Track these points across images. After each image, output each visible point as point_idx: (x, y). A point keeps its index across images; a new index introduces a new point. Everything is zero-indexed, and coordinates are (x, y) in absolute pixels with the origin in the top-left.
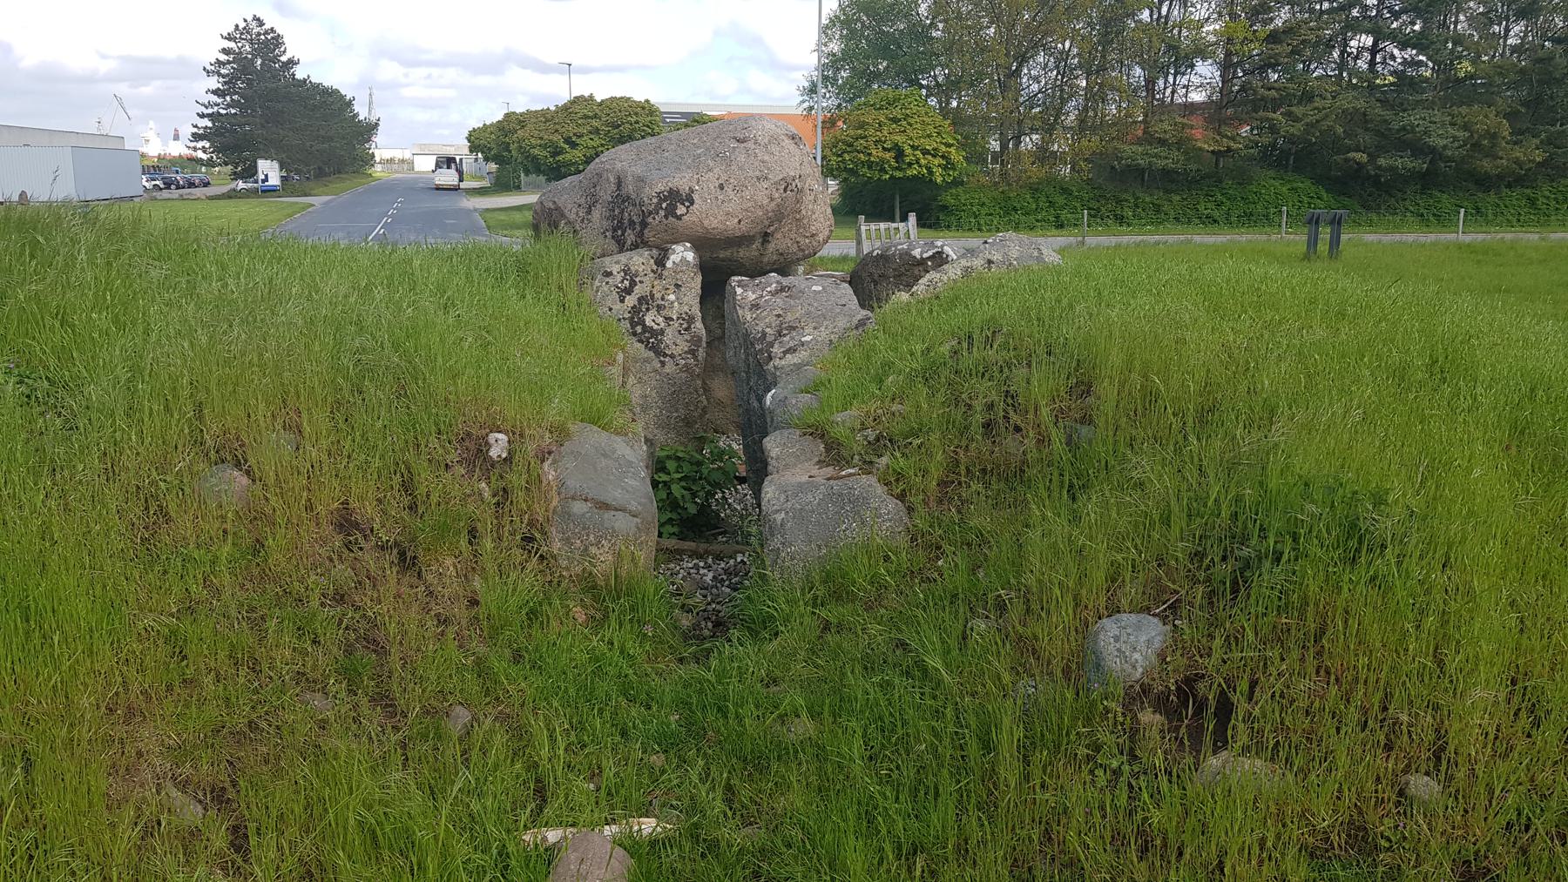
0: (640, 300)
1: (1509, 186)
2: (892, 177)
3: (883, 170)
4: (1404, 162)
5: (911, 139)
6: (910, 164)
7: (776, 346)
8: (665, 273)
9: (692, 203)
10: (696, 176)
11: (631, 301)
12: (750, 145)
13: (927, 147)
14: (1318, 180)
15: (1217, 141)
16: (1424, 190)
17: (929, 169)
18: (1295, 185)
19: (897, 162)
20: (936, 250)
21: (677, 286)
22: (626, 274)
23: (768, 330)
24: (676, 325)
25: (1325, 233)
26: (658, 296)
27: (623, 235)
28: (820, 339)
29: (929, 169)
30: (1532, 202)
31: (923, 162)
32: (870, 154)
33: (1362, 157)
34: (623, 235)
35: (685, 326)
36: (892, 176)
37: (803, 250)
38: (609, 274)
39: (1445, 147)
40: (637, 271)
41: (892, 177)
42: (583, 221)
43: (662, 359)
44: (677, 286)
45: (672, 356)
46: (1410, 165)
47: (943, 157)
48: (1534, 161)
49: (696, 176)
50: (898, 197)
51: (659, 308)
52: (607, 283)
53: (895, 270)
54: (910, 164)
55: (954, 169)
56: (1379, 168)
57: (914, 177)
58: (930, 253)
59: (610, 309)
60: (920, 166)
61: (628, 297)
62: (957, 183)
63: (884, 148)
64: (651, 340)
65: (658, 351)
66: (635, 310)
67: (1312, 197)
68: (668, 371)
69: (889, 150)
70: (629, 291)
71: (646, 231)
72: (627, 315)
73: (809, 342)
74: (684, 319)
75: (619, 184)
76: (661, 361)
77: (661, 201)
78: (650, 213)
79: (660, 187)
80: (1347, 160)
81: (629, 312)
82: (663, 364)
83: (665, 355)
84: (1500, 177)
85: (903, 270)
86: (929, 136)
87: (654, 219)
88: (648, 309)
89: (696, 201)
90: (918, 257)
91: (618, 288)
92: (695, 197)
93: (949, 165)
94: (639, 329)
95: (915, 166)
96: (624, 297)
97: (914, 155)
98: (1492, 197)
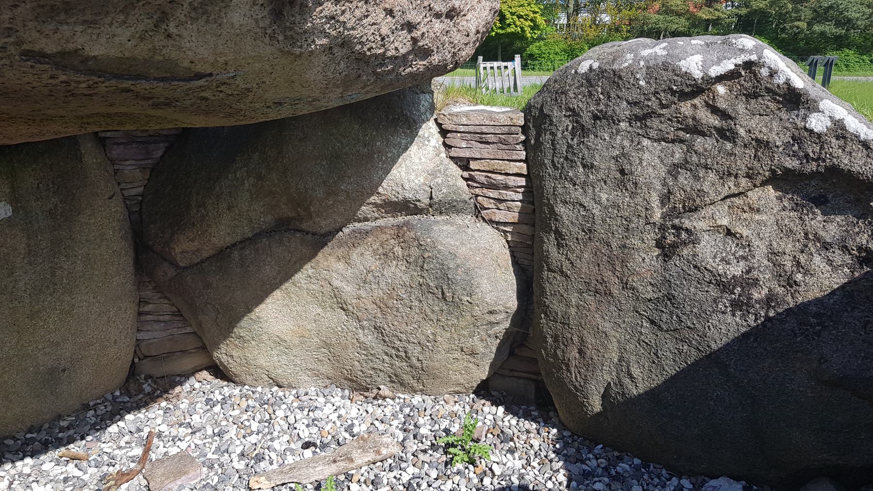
2: (497, 34)
4: (829, 29)
5: (511, 8)
6: (509, 25)
13: (521, 13)
15: (711, 13)
17: (522, 28)
19: (501, 23)
29: (522, 28)
31: (518, 23)
33: (803, 25)
36: (496, 33)
37: (426, 53)
39: (857, 19)
41: (497, 34)
47: (531, 20)
50: (500, 48)
53: (633, 104)
54: (509, 25)
55: (539, 29)
58: (729, 65)
62: (540, 38)
85: (653, 103)
86: (522, 6)
90: (698, 74)
97: (512, 19)
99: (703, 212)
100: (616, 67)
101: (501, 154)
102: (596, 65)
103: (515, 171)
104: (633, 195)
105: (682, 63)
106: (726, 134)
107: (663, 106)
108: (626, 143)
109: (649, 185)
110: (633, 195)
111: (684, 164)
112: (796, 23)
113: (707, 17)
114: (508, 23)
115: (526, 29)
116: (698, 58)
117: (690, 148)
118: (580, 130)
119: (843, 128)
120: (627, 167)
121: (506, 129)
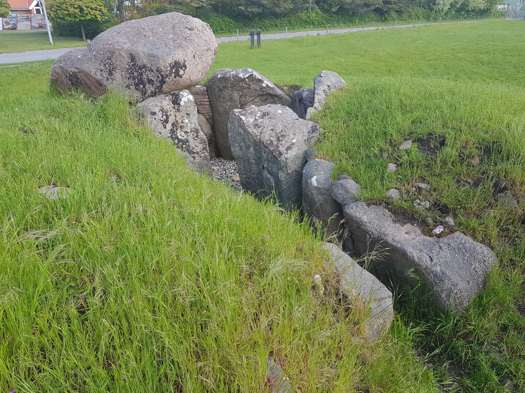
0: (173, 125)
1: (283, 17)
2: (80, 20)
3: (75, 17)
7: (280, 147)
8: (181, 108)
9: (186, 68)
10: (184, 52)
11: (169, 126)
12: (195, 31)
13: (93, 7)
14: (230, 16)
15: (198, 3)
16: (260, 19)
17: (95, 16)
18: (223, 19)
20: (250, 74)
21: (188, 114)
22: (163, 112)
23: (272, 139)
24: (191, 135)
25: (256, 37)
26: (180, 121)
27: (144, 87)
28: (300, 140)
30: (290, 21)
31: (92, 13)
32: (69, 11)
33: (242, 8)
34: (144, 87)
35: (195, 135)
38: (154, 114)
39: (267, 4)
40: (167, 109)
41: (80, 20)
42: (108, 79)
43: (193, 155)
44: (188, 114)
45: (197, 153)
46: (257, 11)
48: (290, 8)
49: (184, 52)
51: (181, 127)
52: (155, 119)
54: (87, 14)
56: (248, 12)
57: (90, 20)
58: (247, 75)
59: (160, 133)
60: (91, 15)
61: (167, 125)
63: (74, 7)
64: (183, 144)
65: (191, 152)
66: (172, 132)
67: (229, 23)
68: (198, 161)
69: (76, 8)
70: (166, 121)
71: (164, 86)
72: (170, 135)
73: (296, 142)
74: (194, 132)
75: (133, 58)
76: (193, 157)
77: (172, 68)
78: (167, 76)
79: (170, 61)
80: (238, 9)
81: (170, 133)
82: (194, 158)
83: (194, 153)
84: (281, 14)
85: (235, 83)
87: (169, 79)
88: (177, 129)
89: (187, 67)
90: (242, 77)
91: (162, 120)
92: (187, 64)
93: (103, 14)
94: (176, 141)
95: (89, 15)
96: (166, 125)
97: (88, 10)
98: (279, 21)
99: (247, 104)
100: (226, 76)
101: (203, 97)
102: (222, 76)
103: (207, 101)
104: (234, 103)
105: (239, 75)
106: (249, 88)
107: (237, 84)
108: (231, 92)
109: (237, 100)
110: (234, 103)
111: (242, 95)
112: (240, 7)
113: (196, 6)
114: (86, 13)
115: (97, 16)
116: (242, 74)
117: (243, 92)
118: (220, 90)
119: (268, 85)
120: (232, 97)
121: (203, 91)
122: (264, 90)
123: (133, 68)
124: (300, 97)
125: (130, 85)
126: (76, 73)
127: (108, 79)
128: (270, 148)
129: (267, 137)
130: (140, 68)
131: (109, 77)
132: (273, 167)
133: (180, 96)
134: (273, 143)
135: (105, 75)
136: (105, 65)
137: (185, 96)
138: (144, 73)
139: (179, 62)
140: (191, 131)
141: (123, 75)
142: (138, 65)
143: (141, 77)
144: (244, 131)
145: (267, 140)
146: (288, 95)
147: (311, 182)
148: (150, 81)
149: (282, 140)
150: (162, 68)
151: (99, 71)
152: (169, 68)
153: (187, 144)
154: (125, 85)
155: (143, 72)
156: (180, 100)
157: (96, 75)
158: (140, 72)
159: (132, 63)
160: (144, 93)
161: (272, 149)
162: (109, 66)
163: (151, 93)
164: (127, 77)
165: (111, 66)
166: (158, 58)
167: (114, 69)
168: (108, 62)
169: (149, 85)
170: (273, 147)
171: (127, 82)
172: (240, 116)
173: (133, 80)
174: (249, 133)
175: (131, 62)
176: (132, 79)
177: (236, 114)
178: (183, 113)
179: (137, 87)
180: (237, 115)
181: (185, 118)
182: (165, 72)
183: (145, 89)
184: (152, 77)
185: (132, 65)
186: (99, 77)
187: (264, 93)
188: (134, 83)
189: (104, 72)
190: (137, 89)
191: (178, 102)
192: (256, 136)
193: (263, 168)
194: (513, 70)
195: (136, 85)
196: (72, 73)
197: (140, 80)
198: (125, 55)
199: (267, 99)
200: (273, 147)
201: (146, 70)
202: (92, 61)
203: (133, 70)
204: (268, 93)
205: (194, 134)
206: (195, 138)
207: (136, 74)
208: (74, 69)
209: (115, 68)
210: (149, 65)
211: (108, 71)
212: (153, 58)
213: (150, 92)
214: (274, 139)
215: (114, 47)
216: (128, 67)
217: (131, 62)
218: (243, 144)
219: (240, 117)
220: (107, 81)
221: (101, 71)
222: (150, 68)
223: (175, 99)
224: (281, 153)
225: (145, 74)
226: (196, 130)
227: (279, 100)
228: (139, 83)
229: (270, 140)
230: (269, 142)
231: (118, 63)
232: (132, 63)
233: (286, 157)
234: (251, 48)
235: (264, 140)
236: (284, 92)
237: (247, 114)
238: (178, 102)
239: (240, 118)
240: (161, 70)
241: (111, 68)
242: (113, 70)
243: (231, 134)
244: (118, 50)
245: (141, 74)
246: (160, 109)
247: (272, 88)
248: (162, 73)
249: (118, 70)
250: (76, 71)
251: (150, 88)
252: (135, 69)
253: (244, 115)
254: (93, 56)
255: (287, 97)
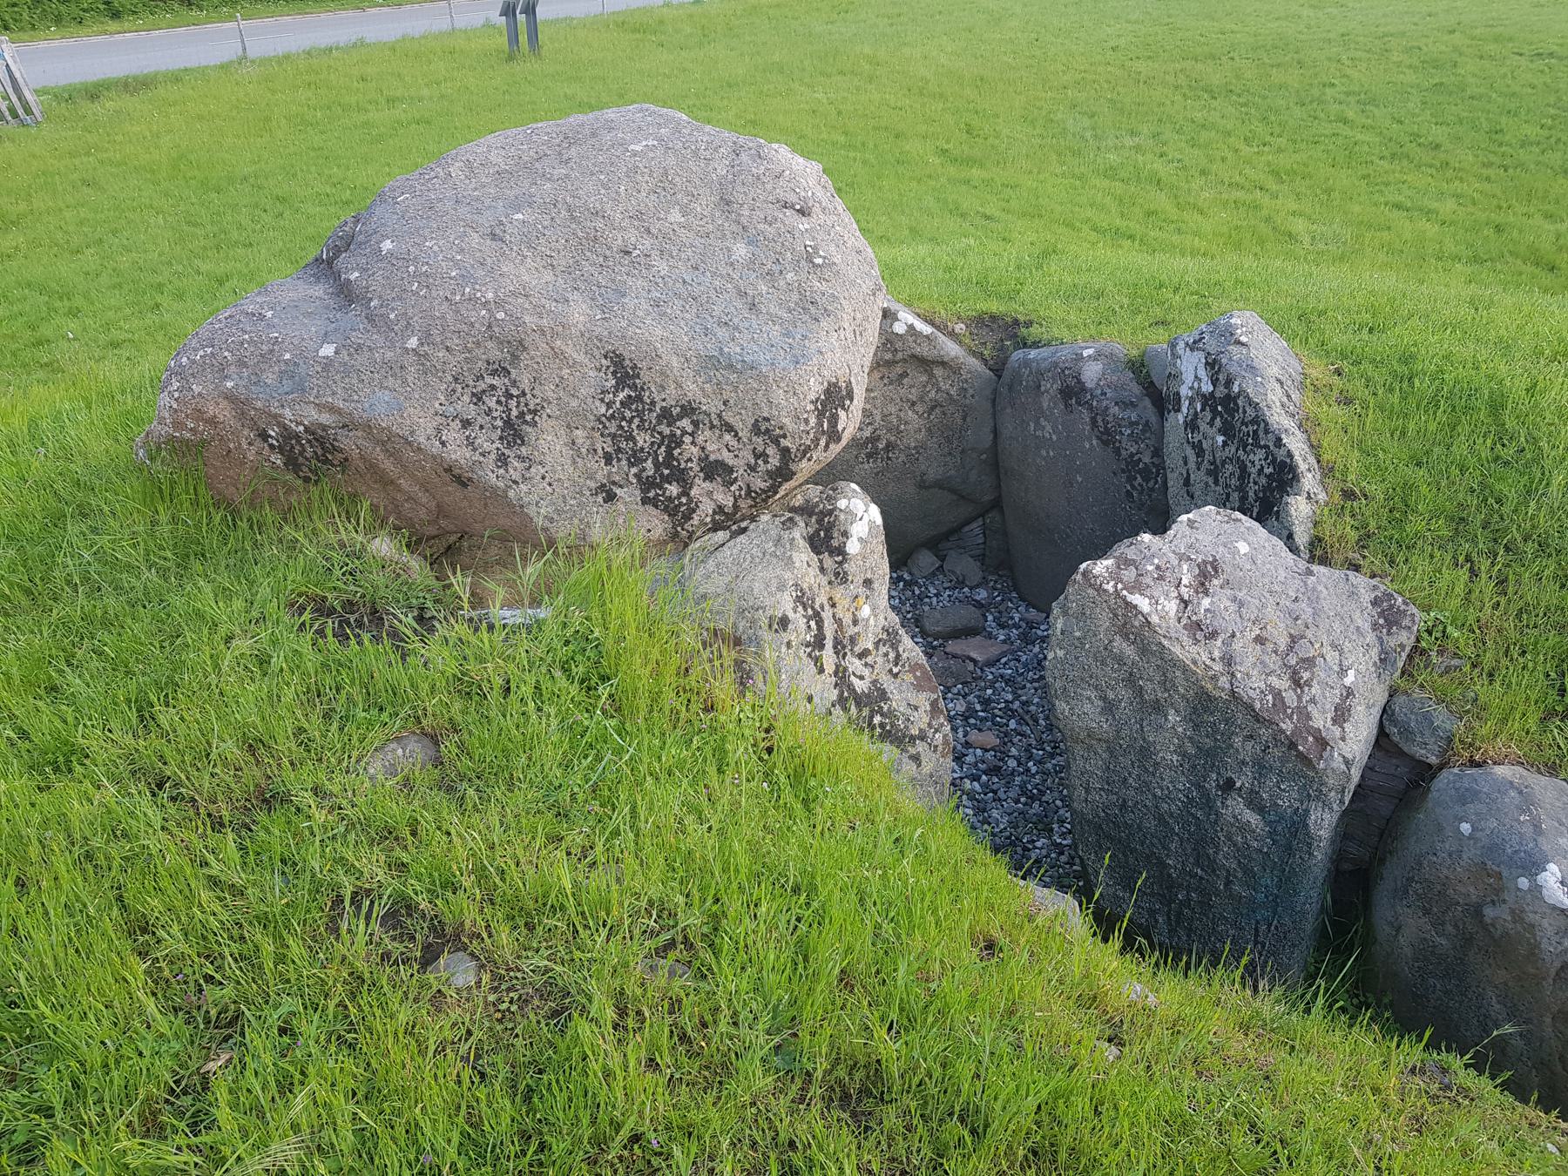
24: (880, 660)
25: (521, 18)
35: (892, 655)
38: (784, 622)
42: (503, 461)
75: (623, 372)
82: (916, 758)
122: (899, 345)
123: (628, 414)
124: (1071, 382)
125: (614, 483)
126: (324, 428)
127: (503, 461)
128: (1284, 726)
129: (1258, 683)
130: (666, 415)
131: (507, 452)
132: (1284, 790)
133: (842, 517)
134: (1284, 703)
135: (489, 442)
136: (480, 399)
137: (859, 516)
138: (687, 439)
139: (835, 385)
140: (877, 644)
141: (580, 441)
142: (653, 403)
143: (669, 454)
144: (1144, 650)
145: (1262, 692)
146: (974, 354)
147: (1537, 889)
148: (714, 470)
149: (1308, 684)
150: (785, 420)
151: (457, 424)
152: (813, 421)
153: (886, 708)
154: (593, 485)
155: (684, 433)
156: (845, 534)
157: (443, 443)
158: (667, 431)
159: (622, 395)
160: (679, 513)
161: (1287, 726)
162: (499, 402)
163: (715, 513)
164: (600, 451)
165: (513, 403)
166: (762, 378)
167: (528, 418)
168: (493, 387)
169: (707, 485)
170: (1291, 718)
171: (602, 472)
172: (1125, 592)
173: (631, 465)
174: (1175, 663)
175: (617, 389)
176: (624, 462)
177: (1105, 586)
178: (856, 587)
179: (651, 494)
180: (1111, 590)
181: (861, 600)
182: (801, 438)
183: (690, 500)
184: (725, 453)
185: (622, 403)
186: (458, 453)
187: (900, 356)
188: (635, 475)
189: (481, 427)
190: (654, 502)
191: (835, 543)
192: (1214, 678)
193: (1229, 785)
194: (1298, 112)
195: (646, 484)
196: (301, 428)
197: (667, 464)
198: (581, 357)
199: (904, 375)
200: (1291, 718)
201: (696, 424)
202: (410, 379)
203: (630, 422)
204: (913, 356)
205: (886, 655)
206: (895, 670)
207: (643, 440)
208: (312, 415)
209: (535, 412)
210: (711, 406)
211: (499, 423)
212: (733, 377)
213: (711, 512)
214: (1282, 683)
215: (518, 322)
216: (603, 410)
217: (617, 389)
218: (1125, 693)
219: (1124, 599)
220: (502, 471)
221: (466, 424)
222: (720, 416)
223: (817, 531)
224: (1323, 739)
225: (693, 443)
226: (888, 634)
227: (949, 377)
228: (662, 475)
229: (1272, 689)
230: (1270, 697)
231: (549, 390)
232: (622, 395)
233: (1350, 756)
234: (511, 58)
235: (1251, 693)
236: (960, 343)
237: (1148, 580)
238: (835, 543)
239: (1128, 604)
240: (781, 428)
241: (514, 413)
242: (526, 422)
243: (1060, 653)
244: (543, 333)
245: (675, 442)
246: (794, 594)
247: (927, 337)
248: (785, 443)
249: (552, 422)
250: (326, 418)
251: (708, 497)
252: (642, 421)
253: (1137, 587)
254: (412, 358)
255: (974, 363)
